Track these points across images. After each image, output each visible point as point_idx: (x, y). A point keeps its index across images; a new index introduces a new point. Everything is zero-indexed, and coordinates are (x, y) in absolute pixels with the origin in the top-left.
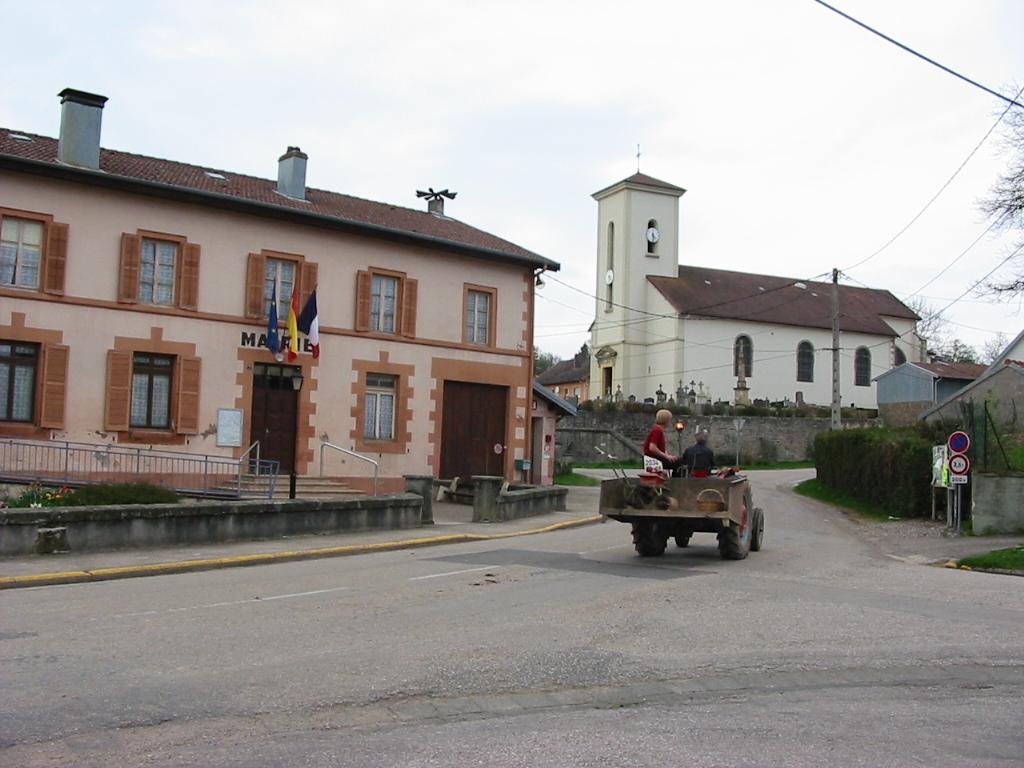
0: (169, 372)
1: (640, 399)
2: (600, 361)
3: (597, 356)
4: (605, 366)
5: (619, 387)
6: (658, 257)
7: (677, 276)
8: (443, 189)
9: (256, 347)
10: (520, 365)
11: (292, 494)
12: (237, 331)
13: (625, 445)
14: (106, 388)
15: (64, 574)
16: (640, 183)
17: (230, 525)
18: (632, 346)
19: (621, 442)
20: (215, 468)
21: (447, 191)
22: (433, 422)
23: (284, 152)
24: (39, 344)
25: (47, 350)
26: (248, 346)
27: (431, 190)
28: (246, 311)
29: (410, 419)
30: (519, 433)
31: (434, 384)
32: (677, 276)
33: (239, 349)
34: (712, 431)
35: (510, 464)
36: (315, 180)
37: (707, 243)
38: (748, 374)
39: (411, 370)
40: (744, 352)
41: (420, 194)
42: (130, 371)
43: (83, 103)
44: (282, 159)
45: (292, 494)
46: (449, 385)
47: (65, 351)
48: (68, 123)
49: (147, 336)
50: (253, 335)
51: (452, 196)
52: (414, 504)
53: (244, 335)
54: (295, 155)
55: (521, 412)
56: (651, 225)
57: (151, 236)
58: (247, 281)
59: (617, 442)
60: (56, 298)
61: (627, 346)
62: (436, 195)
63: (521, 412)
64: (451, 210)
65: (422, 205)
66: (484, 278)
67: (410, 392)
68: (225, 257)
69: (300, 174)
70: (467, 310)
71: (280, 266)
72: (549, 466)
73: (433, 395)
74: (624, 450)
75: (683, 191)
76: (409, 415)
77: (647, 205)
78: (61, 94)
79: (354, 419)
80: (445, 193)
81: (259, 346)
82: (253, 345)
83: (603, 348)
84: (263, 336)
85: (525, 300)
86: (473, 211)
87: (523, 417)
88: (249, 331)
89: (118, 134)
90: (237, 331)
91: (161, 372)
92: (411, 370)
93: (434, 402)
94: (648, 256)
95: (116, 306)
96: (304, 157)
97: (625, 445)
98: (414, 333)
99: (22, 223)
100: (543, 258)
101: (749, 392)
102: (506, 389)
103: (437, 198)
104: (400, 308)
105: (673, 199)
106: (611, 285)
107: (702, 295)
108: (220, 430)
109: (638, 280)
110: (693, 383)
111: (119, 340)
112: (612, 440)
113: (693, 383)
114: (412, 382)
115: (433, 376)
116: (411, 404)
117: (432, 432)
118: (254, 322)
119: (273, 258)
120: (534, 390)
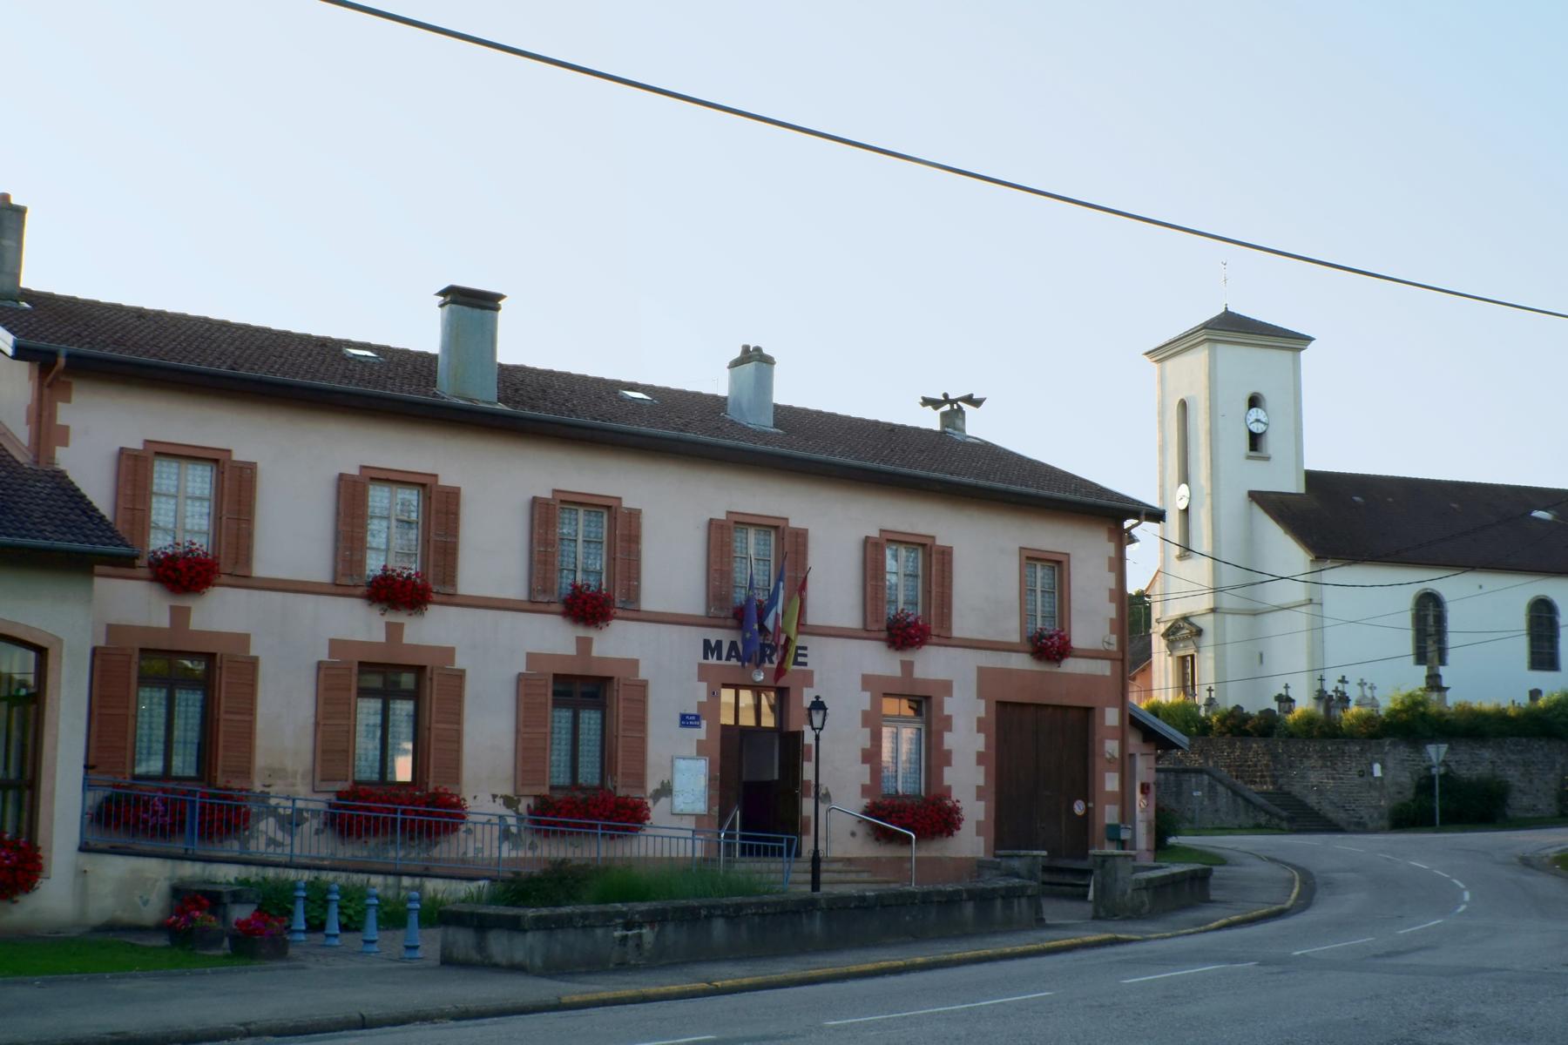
0: (206, 684)
1: (1252, 708)
2: (1172, 645)
3: (1166, 635)
4: (1182, 653)
5: (1210, 690)
6: (1267, 459)
7: (1302, 490)
8: (966, 393)
9: (723, 662)
10: (1108, 673)
11: (816, 884)
12: (693, 639)
13: (1236, 793)
14: (517, 731)
15: (604, 995)
16: (1231, 327)
17: (817, 925)
18: (1229, 617)
19: (1228, 787)
20: (666, 848)
21: (971, 396)
22: (982, 768)
23: (737, 354)
24: (214, 655)
25: (435, 678)
26: (713, 660)
27: (946, 395)
28: (708, 607)
29: (949, 764)
30: (1112, 783)
31: (980, 708)
32: (1302, 490)
33: (700, 665)
34: (1390, 764)
35: (1098, 831)
36: (790, 390)
37: (1356, 430)
38: (1442, 662)
39: (946, 687)
40: (1429, 622)
41: (927, 402)
42: (354, 691)
43: (472, 305)
44: (735, 364)
45: (816, 884)
46: (1003, 707)
47: (460, 675)
48: (453, 334)
49: (571, 650)
50: (719, 643)
51: (977, 403)
52: (1029, 892)
53: (707, 643)
54: (754, 359)
55: (1112, 747)
56: (1254, 402)
57: (595, 501)
58: (532, 520)
59: (1221, 789)
60: (445, 599)
61: (1220, 616)
62: (952, 402)
63: (1112, 747)
64: (977, 426)
65: (931, 420)
66: (1049, 536)
67: (947, 723)
68: (675, 519)
69: (764, 383)
70: (1026, 590)
71: (752, 533)
72: (1149, 832)
73: (981, 725)
74: (1235, 801)
75: (1309, 339)
76: (946, 759)
77: (1248, 365)
78: (443, 293)
79: (867, 767)
80: (969, 400)
81: (728, 659)
82: (719, 658)
83: (1177, 620)
84: (733, 645)
85: (1110, 570)
86: (1018, 424)
87: (1117, 755)
88: (714, 635)
89: (520, 342)
90: (696, 636)
91: (190, 681)
92: (946, 687)
93: (982, 737)
94: (1249, 458)
95: (528, 606)
96: (768, 361)
97: (1236, 793)
98: (950, 629)
99: (394, 487)
100: (1139, 503)
101: (1448, 693)
102: (1087, 712)
103: (953, 409)
104: (927, 592)
105: (1289, 354)
106: (1186, 511)
107: (1346, 519)
108: (677, 787)
109: (1235, 499)
110: (1343, 681)
111: (532, 658)
112: (1212, 788)
113: (1343, 681)
114: (950, 706)
115: (980, 695)
116: (950, 740)
117: (981, 782)
118: (721, 622)
119: (741, 522)
120: (1131, 717)
